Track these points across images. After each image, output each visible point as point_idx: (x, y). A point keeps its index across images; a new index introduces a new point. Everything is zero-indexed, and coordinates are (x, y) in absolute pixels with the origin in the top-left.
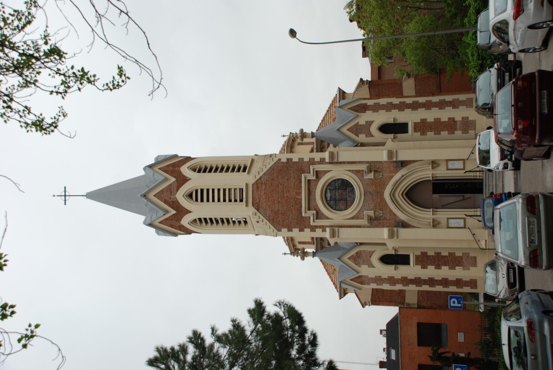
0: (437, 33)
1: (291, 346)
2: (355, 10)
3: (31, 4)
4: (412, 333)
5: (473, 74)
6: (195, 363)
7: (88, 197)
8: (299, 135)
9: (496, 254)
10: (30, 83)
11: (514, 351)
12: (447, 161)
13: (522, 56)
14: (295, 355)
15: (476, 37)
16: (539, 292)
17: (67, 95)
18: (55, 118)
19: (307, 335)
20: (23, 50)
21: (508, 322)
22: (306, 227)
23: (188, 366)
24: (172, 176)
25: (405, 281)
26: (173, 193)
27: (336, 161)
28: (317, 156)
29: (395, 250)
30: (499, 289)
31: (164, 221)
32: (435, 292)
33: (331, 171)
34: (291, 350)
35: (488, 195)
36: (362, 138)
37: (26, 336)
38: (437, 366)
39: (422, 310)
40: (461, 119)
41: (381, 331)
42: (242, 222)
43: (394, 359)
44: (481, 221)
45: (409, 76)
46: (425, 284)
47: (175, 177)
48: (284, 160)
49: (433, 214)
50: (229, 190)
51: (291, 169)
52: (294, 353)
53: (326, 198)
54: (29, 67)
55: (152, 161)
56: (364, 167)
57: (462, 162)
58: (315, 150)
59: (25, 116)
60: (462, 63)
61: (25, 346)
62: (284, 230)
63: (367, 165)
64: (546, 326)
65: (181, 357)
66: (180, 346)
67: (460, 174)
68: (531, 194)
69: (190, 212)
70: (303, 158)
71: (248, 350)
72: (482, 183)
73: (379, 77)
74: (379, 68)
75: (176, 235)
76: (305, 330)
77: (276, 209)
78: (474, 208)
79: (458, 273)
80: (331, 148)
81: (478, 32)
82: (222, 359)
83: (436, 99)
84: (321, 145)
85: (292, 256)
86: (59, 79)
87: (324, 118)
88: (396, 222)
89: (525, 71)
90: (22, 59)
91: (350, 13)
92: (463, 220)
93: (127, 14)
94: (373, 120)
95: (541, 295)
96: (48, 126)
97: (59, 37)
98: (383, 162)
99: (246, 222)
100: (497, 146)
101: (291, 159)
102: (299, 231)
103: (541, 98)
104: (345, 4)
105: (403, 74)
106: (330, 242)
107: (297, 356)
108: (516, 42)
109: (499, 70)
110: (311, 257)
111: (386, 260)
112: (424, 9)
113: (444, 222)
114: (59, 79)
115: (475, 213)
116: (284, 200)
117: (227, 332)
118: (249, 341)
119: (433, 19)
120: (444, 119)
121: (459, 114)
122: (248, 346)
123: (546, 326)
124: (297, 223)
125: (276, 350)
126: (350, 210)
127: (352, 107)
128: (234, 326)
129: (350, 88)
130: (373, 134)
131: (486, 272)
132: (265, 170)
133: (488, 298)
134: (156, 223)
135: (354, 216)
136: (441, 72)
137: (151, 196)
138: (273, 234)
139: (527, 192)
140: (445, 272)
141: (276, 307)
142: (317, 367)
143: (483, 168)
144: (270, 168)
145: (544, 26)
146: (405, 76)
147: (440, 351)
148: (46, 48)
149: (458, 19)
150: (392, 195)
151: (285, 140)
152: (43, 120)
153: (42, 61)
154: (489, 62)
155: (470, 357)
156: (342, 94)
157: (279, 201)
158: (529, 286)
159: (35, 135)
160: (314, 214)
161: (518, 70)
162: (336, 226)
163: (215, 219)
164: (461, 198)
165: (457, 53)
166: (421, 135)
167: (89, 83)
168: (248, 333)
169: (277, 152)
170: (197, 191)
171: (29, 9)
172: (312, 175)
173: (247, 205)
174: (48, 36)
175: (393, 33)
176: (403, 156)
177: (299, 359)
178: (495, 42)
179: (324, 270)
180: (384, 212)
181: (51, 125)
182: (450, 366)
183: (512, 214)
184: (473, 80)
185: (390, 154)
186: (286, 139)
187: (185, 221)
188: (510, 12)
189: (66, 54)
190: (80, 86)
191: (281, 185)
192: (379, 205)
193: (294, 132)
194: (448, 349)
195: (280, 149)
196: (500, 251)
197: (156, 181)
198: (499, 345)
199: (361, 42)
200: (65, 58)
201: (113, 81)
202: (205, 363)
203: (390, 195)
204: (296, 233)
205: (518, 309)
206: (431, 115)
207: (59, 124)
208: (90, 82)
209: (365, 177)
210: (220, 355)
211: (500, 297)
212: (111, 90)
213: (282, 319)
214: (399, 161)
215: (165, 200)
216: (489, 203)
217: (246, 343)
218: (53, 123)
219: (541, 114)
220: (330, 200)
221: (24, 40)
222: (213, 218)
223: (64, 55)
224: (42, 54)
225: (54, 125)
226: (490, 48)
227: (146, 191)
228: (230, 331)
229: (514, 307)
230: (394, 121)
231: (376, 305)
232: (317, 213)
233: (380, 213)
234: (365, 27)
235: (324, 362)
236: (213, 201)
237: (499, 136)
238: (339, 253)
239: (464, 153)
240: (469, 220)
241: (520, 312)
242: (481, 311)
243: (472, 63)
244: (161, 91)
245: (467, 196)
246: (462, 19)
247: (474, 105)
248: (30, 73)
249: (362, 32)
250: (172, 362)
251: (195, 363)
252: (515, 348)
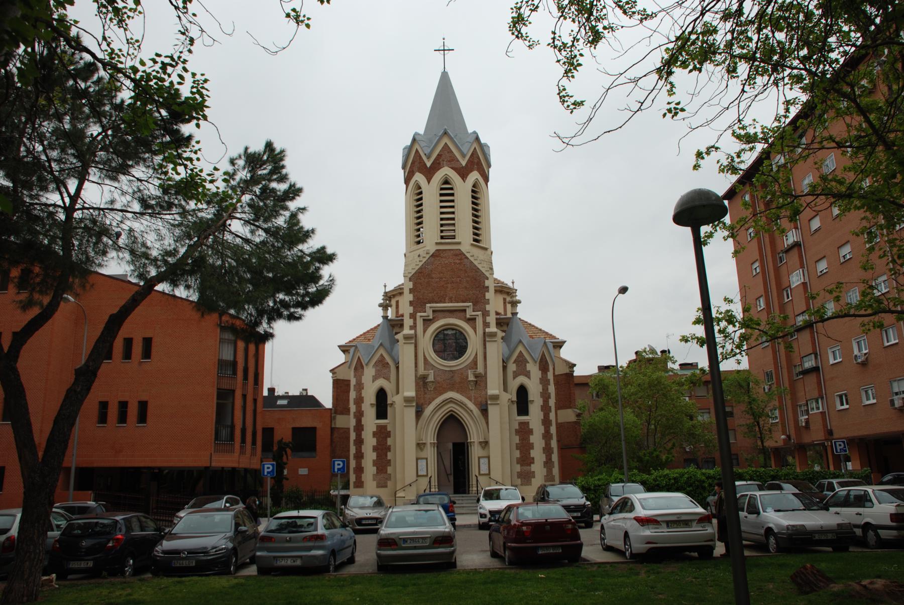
0: (623, 443)
1: (288, 293)
2: (647, 356)
3: (644, 15)
4: (306, 422)
5: (579, 481)
6: (268, 191)
7: (442, 73)
8: (514, 299)
9: (390, 507)
10: (562, 12)
11: (292, 522)
12: (489, 457)
13: (597, 528)
14: (278, 297)
15: (618, 482)
16: (353, 548)
17: (552, 49)
18: (527, 37)
19: (299, 310)
20: (596, 5)
21: (322, 516)
23: (265, 184)
24: (468, 162)
25: (359, 415)
26: (449, 163)
27: (487, 339)
28: (492, 319)
29: (392, 404)
30: (354, 510)
32: (349, 446)
34: (283, 293)
35: (452, 499)
36: (512, 367)
37: (298, 16)
38: (273, 447)
39: (329, 432)
40: (532, 470)
41: (306, 390)
42: (419, 239)
43: (278, 403)
44: (425, 491)
45: (578, 415)
46: (357, 435)
47: (466, 165)
48: (487, 283)
49: (431, 443)
50: (454, 225)
52: (281, 296)
53: (447, 329)
54: (579, 11)
55: (483, 141)
56: (480, 369)
57: (487, 472)
58: (498, 317)
59: (528, 6)
60: (591, 470)
61: (288, 15)
62: (411, 285)
63: (483, 373)
64: (320, 552)
65: (275, 177)
66: (286, 175)
67: (474, 470)
68: (454, 540)
69: (429, 183)
70: (489, 304)
71: (283, 247)
72: (465, 493)
73: (577, 385)
74: (586, 385)
75: (404, 167)
76: (304, 308)
77: (434, 276)
78: (438, 485)
79: (370, 470)
80: (501, 334)
81: (623, 484)
82: (273, 220)
83: (554, 444)
84: (504, 323)
85: (383, 294)
86: (568, 40)
87: (533, 326)
88: (422, 404)
89: (581, 531)
90: (587, 4)
91: (645, 351)
92: (425, 474)
93: (639, 109)
94: (431, 183)
95: (351, 549)
96: (518, 29)
97: (611, 41)
99: (419, 243)
100: (504, 507)
101: (488, 291)
103: (554, 547)
104: (654, 346)
105: (580, 410)
106: (399, 334)
107: (278, 300)
108: (612, 521)
109: (584, 506)
110: (382, 314)
111: (381, 395)
112: (648, 429)
113: (423, 454)
114: (568, 40)
115: (433, 487)
117: (301, 225)
118: (292, 248)
119: (638, 439)
120: (533, 453)
121: (538, 468)
122: (286, 246)
123: (320, 552)
124: (418, 299)
125: (283, 277)
126: (434, 355)
127: (545, 355)
128: (308, 231)
129: (565, 353)
130: (516, 379)
131: (372, 497)
132: (476, 263)
133: (345, 499)
134: (416, 146)
136: (582, 448)
137: (445, 140)
138: (407, 272)
139: (456, 537)
140: (370, 456)
141: (329, 276)
142: (266, 321)
143: (481, 493)
144: (478, 269)
145: (627, 547)
146: (579, 411)
147: (288, 450)
148: (600, 27)
149: (636, 464)
150: (451, 400)
151: (509, 284)
152: (524, 24)
153: (586, 24)
154: (592, 496)
155: (284, 480)
156: (559, 345)
157: (442, 278)
158: (359, 538)
159: (508, 17)
160: (428, 316)
161: (583, 525)
162: (416, 341)
163: (422, 210)
164: (449, 472)
165: (602, 464)
166: (516, 430)
167: (566, 71)
168: (300, 247)
169: (495, 276)
170: (452, 189)
171: (638, 13)
173: (437, 244)
174: (612, 30)
175: (623, 397)
176: (493, 411)
177: (275, 302)
178: (613, 501)
179: (369, 329)
181: (519, 32)
182: (274, 460)
183: (433, 522)
184: (573, 481)
185: (495, 398)
186: (510, 285)
187: (419, 177)
188: (643, 513)
189: (595, 48)
190: (562, 62)
191: (460, 281)
193: (517, 294)
194: (290, 458)
195: (499, 279)
196: (394, 510)
197: (462, 145)
198: (298, 508)
199: (615, 364)
200: (591, 46)
201: (568, 96)
202: (269, 201)
203: (451, 398)
204: (408, 297)
205: (335, 527)
206: (537, 439)
207: (520, 40)
208: (566, 72)
209: (469, 371)
210: (277, 217)
211: (346, 510)
212: (559, 94)
213: (316, 282)
214: (487, 407)
216: (444, 500)
217: (290, 244)
218: (522, 34)
219: (537, 548)
220: (444, 335)
221: (606, 6)
222: (423, 207)
223: (593, 46)
224: (593, 23)
225: (520, 35)
226: (607, 496)
227: (451, 135)
228: (302, 228)
229: (337, 523)
231: (333, 385)
232: (430, 320)
233: (431, 387)
234: (630, 368)
235: (273, 328)
236: (441, 207)
237: (515, 508)
238: (387, 344)
239: (496, 474)
240: (427, 479)
241: (332, 528)
242: (332, 492)
243: (591, 480)
244: (559, 145)
245: (451, 478)
246: (636, 468)
247: (547, 483)
248: (573, 12)
249: (625, 365)
250: (270, 167)
251: (268, 191)
252: (295, 522)
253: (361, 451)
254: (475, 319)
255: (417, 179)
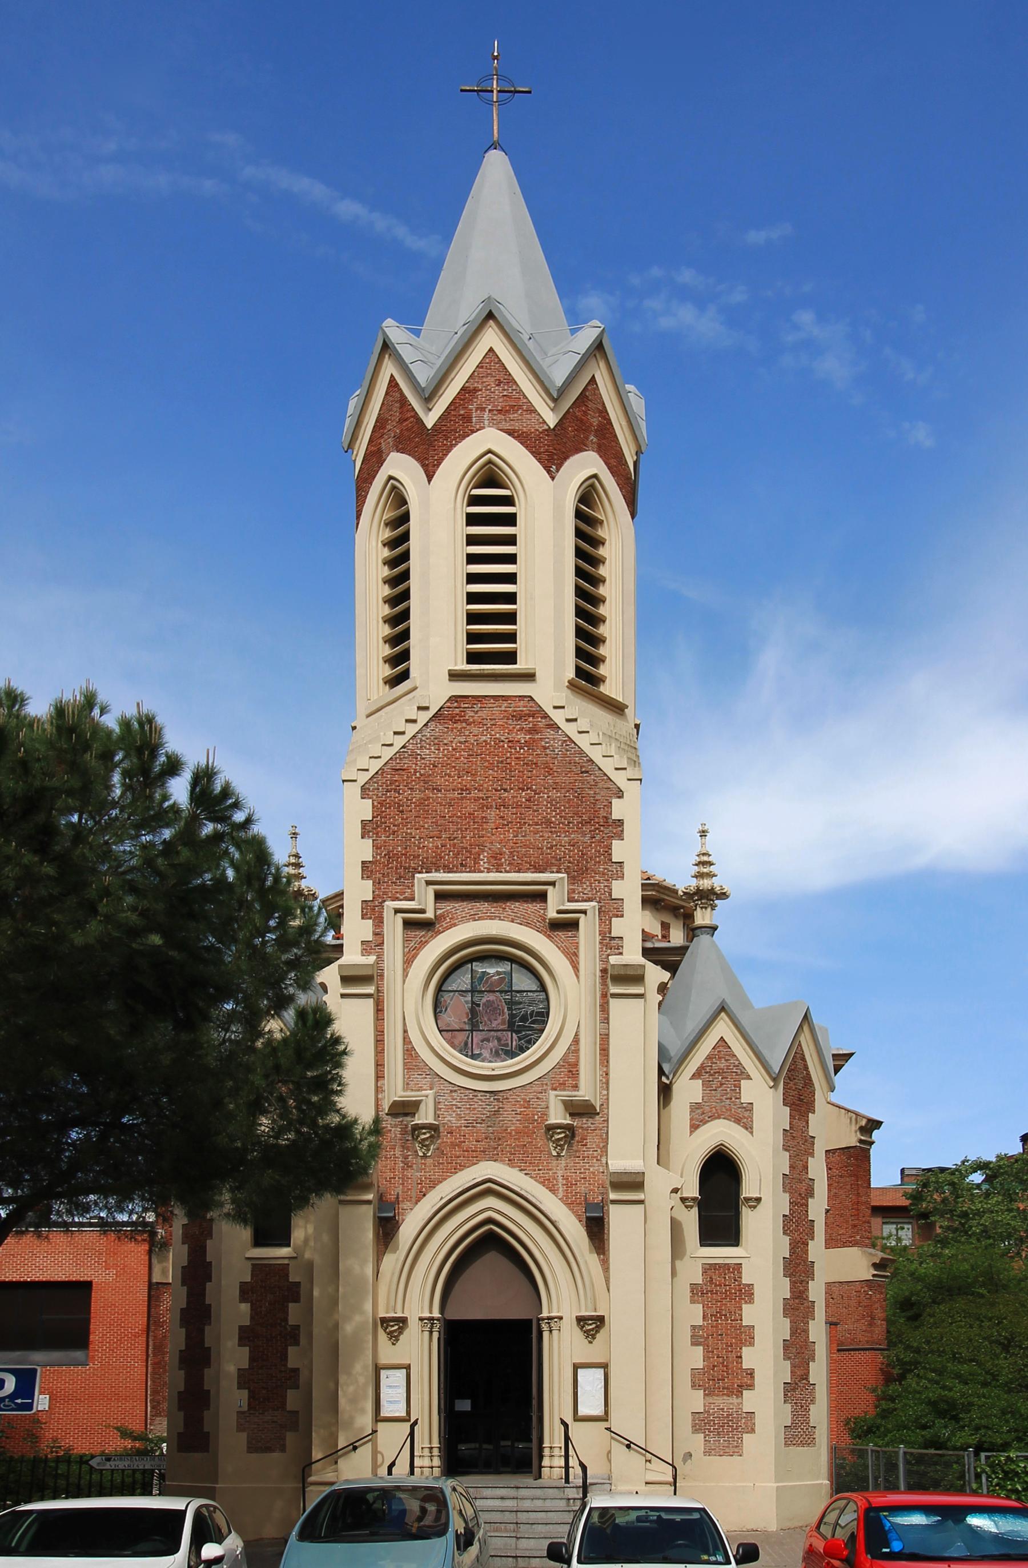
22: (377, 884)
31: (397, 395)
33: (578, 977)
49: (421, 1319)
51: (584, 835)
83: (817, 1331)
92: (403, 1414)
98: (604, 1160)
102: (363, 862)
116: (471, 807)
120: (750, 1357)
127: (803, 1059)
135: (417, 1056)
150: (489, 1189)
160: (423, 911)
170: (508, 501)
172: (562, 908)
173: (455, 676)
180: (429, 1161)
192: (453, 1145)
203: (490, 1180)
215: (476, 390)
230: (748, 1199)
240: (406, 1427)
253: (203, 1341)
254: (574, 925)
255: (392, 473)
